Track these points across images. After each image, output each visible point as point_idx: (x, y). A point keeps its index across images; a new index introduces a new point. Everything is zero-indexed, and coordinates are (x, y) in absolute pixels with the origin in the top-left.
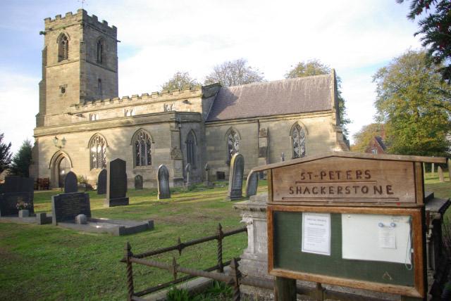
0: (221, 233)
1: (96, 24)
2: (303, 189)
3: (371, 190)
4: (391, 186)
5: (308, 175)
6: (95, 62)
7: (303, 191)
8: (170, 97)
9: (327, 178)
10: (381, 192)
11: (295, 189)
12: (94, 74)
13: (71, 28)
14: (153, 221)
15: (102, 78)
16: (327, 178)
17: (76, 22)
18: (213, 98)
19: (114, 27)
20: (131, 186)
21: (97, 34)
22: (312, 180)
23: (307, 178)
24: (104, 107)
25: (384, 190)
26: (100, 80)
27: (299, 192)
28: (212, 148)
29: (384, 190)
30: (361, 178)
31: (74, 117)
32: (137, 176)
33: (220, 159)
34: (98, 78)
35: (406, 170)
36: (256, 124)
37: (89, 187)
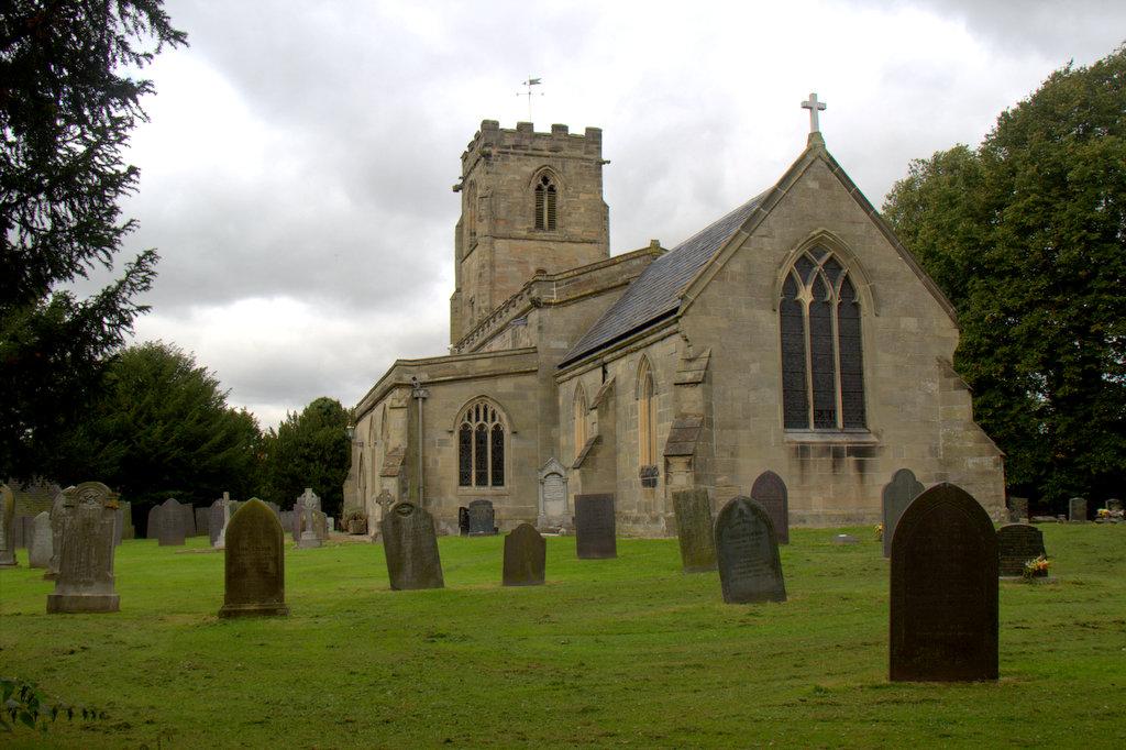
19: (588, 130)
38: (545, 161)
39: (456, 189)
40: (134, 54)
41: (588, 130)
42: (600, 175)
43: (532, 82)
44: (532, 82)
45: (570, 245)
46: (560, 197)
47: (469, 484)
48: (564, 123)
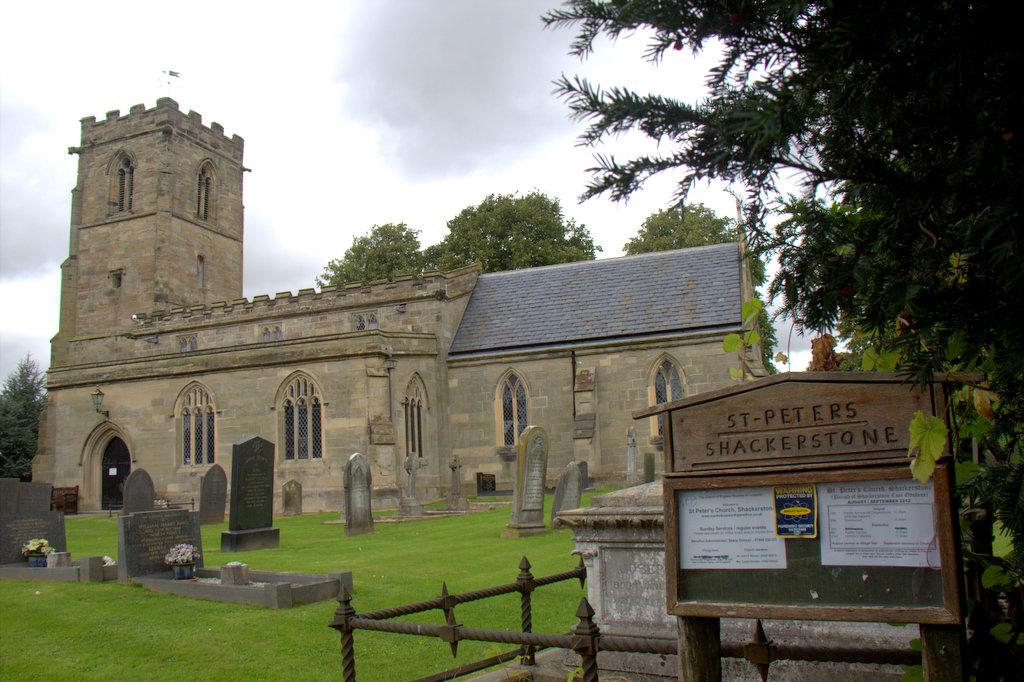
0: (530, 578)
1: (197, 131)
2: (733, 445)
3: (859, 439)
4: (892, 428)
5: (742, 418)
6: (191, 217)
7: (731, 451)
8: (365, 299)
9: (776, 422)
10: (875, 440)
11: (716, 448)
12: (189, 245)
13: (142, 140)
14: (350, 574)
15: (208, 255)
16: (776, 422)
17: (152, 127)
18: (466, 299)
19: (235, 136)
20: (278, 504)
21: (199, 156)
22: (748, 428)
23: (740, 425)
24: (212, 321)
25: (882, 435)
26: (201, 258)
27: (724, 451)
28: (465, 418)
29: (882, 435)
30: (839, 416)
31: (139, 344)
32: (289, 484)
33: (480, 444)
34: (196, 253)
35: (918, 398)
36: (569, 361)
37: (784, 255)
38: (209, 155)
39: (72, 151)
40: (553, 20)
41: (235, 136)
42: (241, 181)
43: (172, 73)
44: (172, 73)
45: (221, 237)
46: (214, 191)
47: (306, 457)
48: (115, 109)
